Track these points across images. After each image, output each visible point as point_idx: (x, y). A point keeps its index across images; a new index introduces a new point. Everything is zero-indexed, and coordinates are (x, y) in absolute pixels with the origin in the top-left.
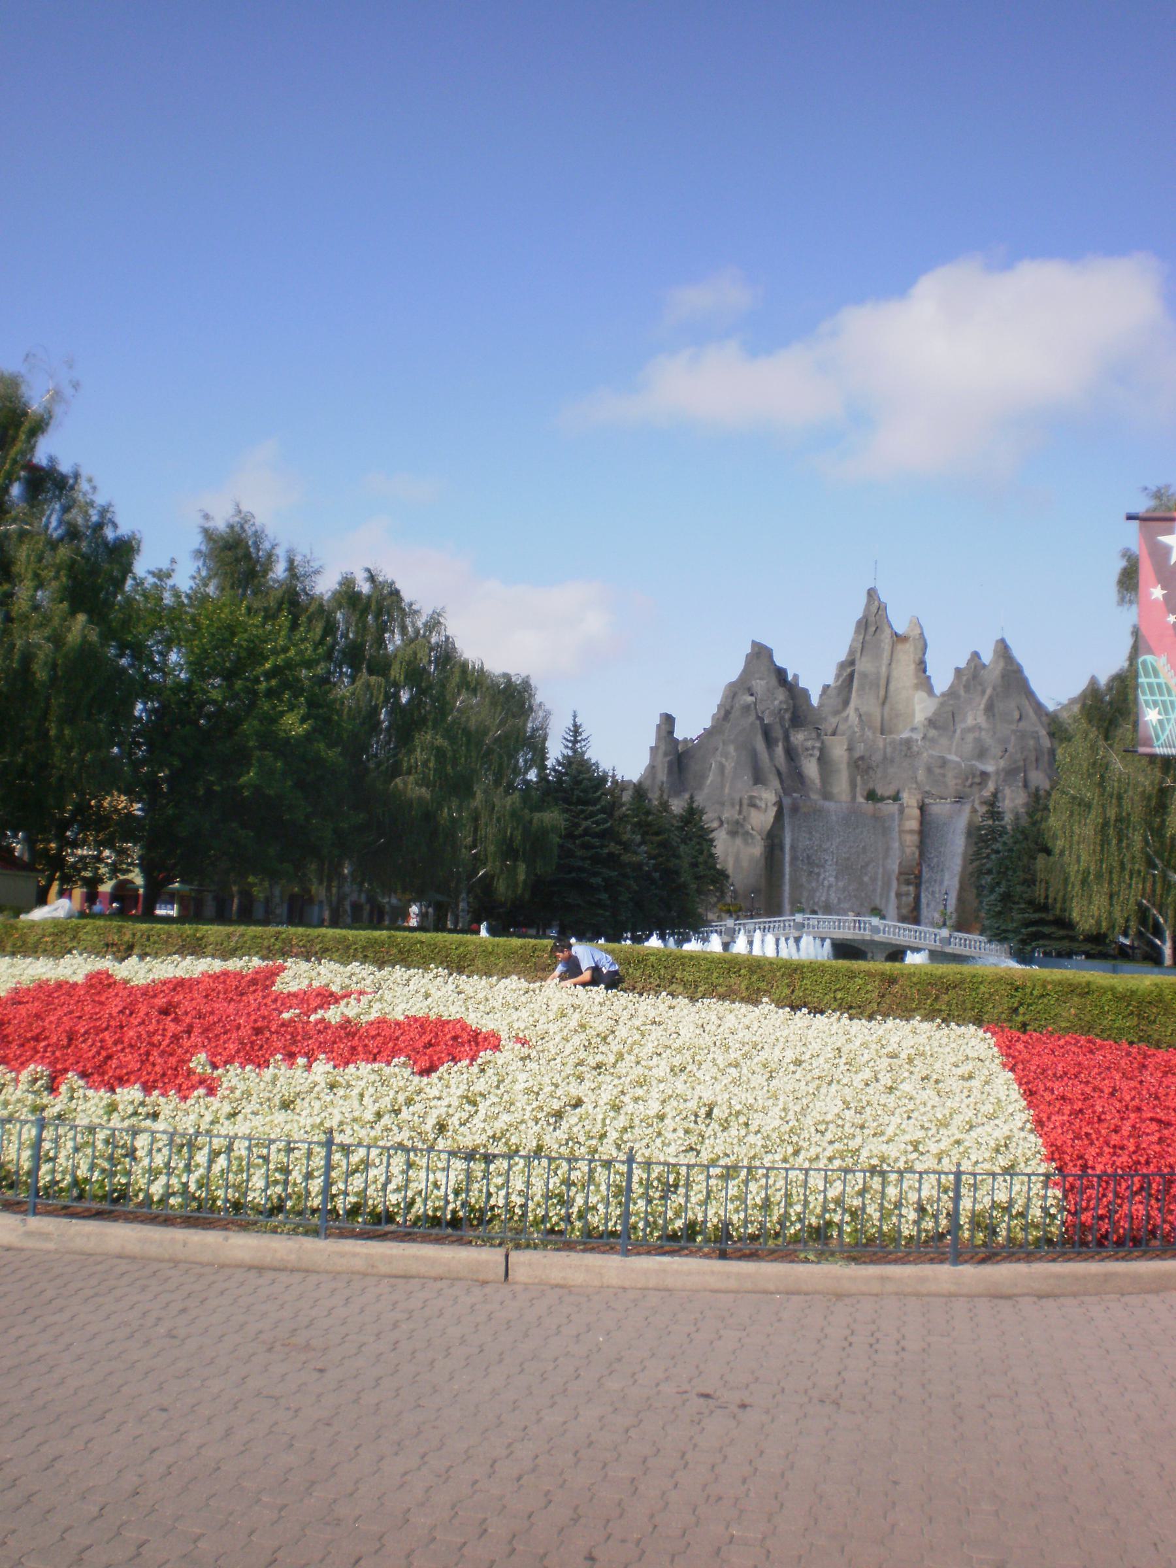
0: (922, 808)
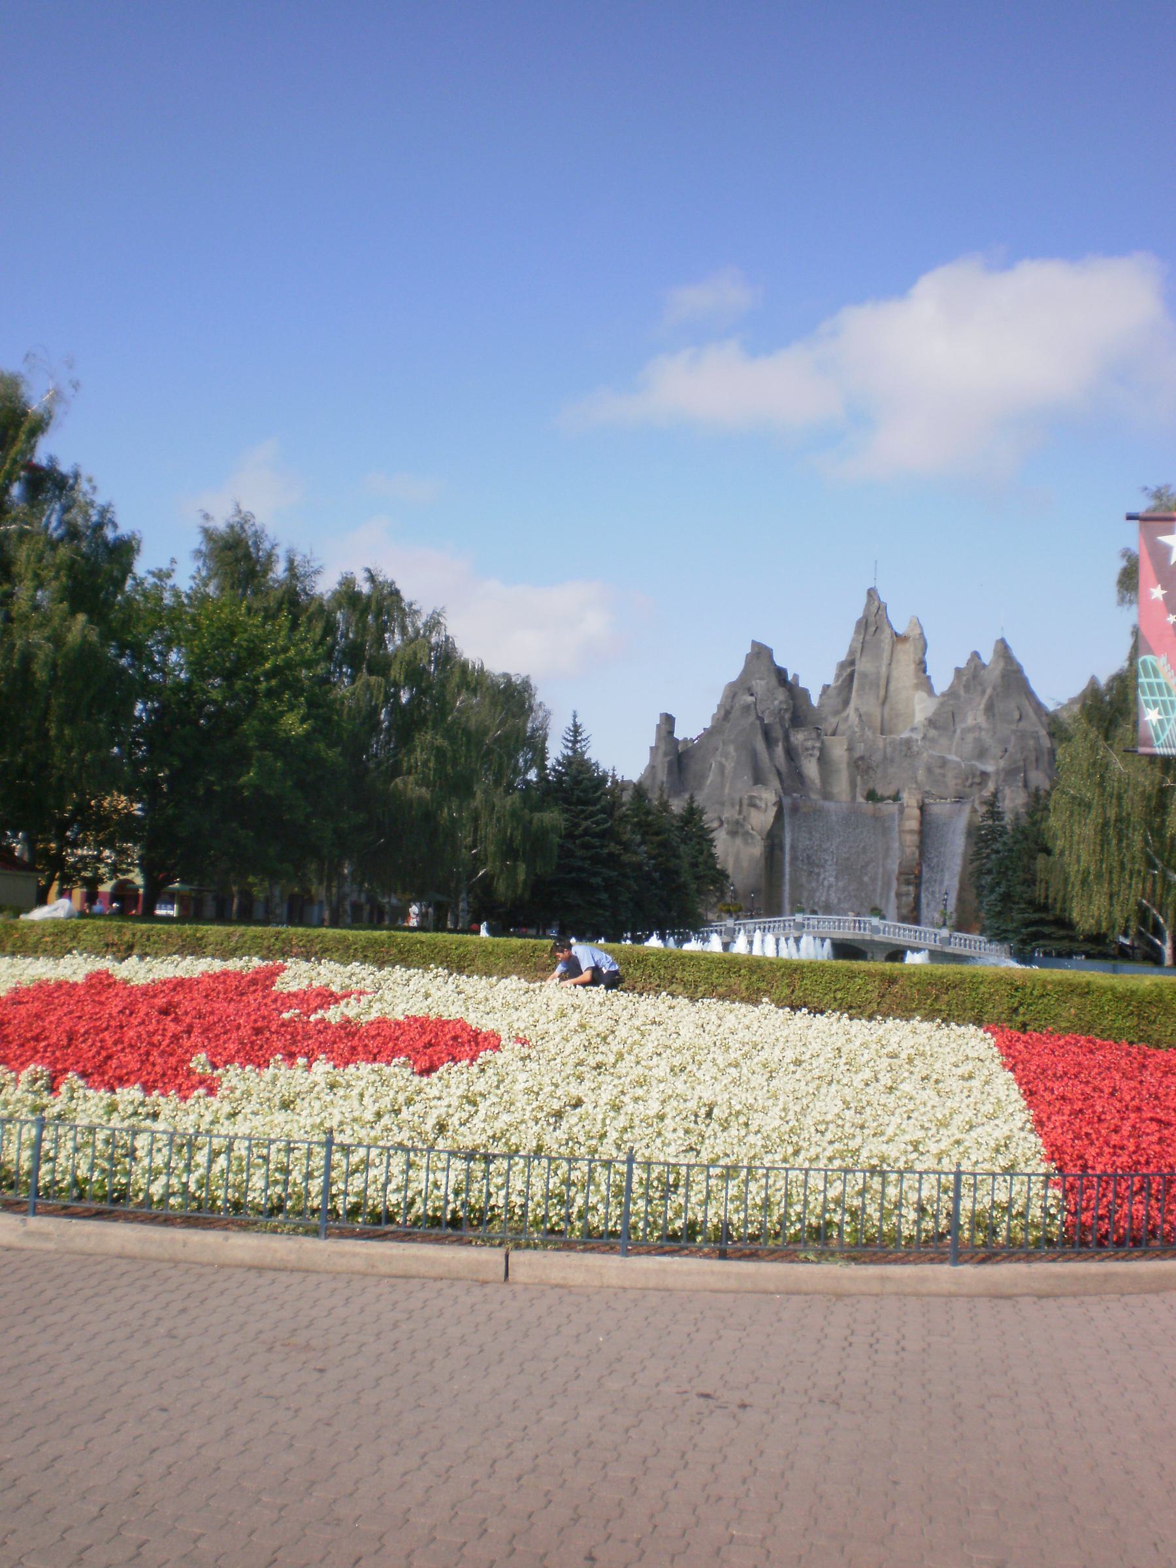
0: (922, 808)
